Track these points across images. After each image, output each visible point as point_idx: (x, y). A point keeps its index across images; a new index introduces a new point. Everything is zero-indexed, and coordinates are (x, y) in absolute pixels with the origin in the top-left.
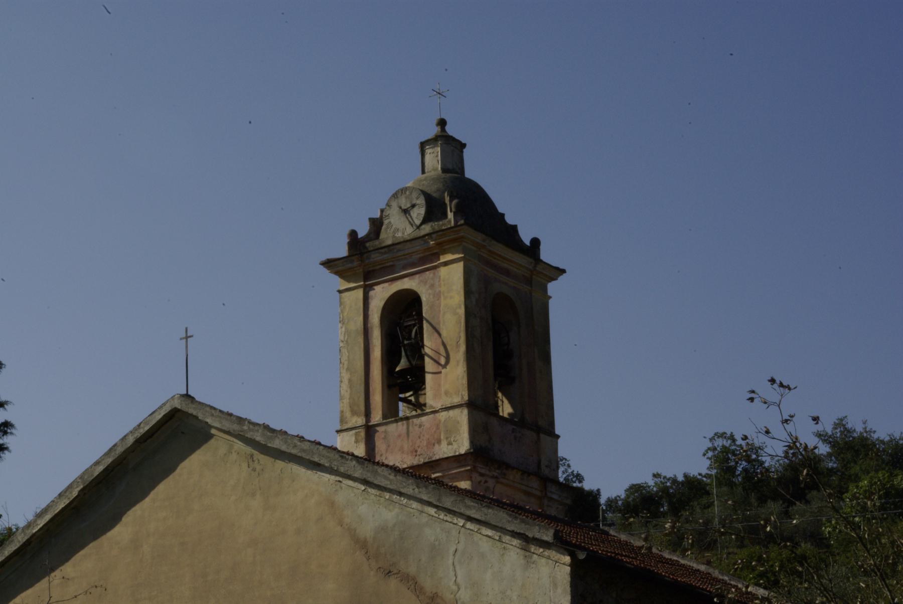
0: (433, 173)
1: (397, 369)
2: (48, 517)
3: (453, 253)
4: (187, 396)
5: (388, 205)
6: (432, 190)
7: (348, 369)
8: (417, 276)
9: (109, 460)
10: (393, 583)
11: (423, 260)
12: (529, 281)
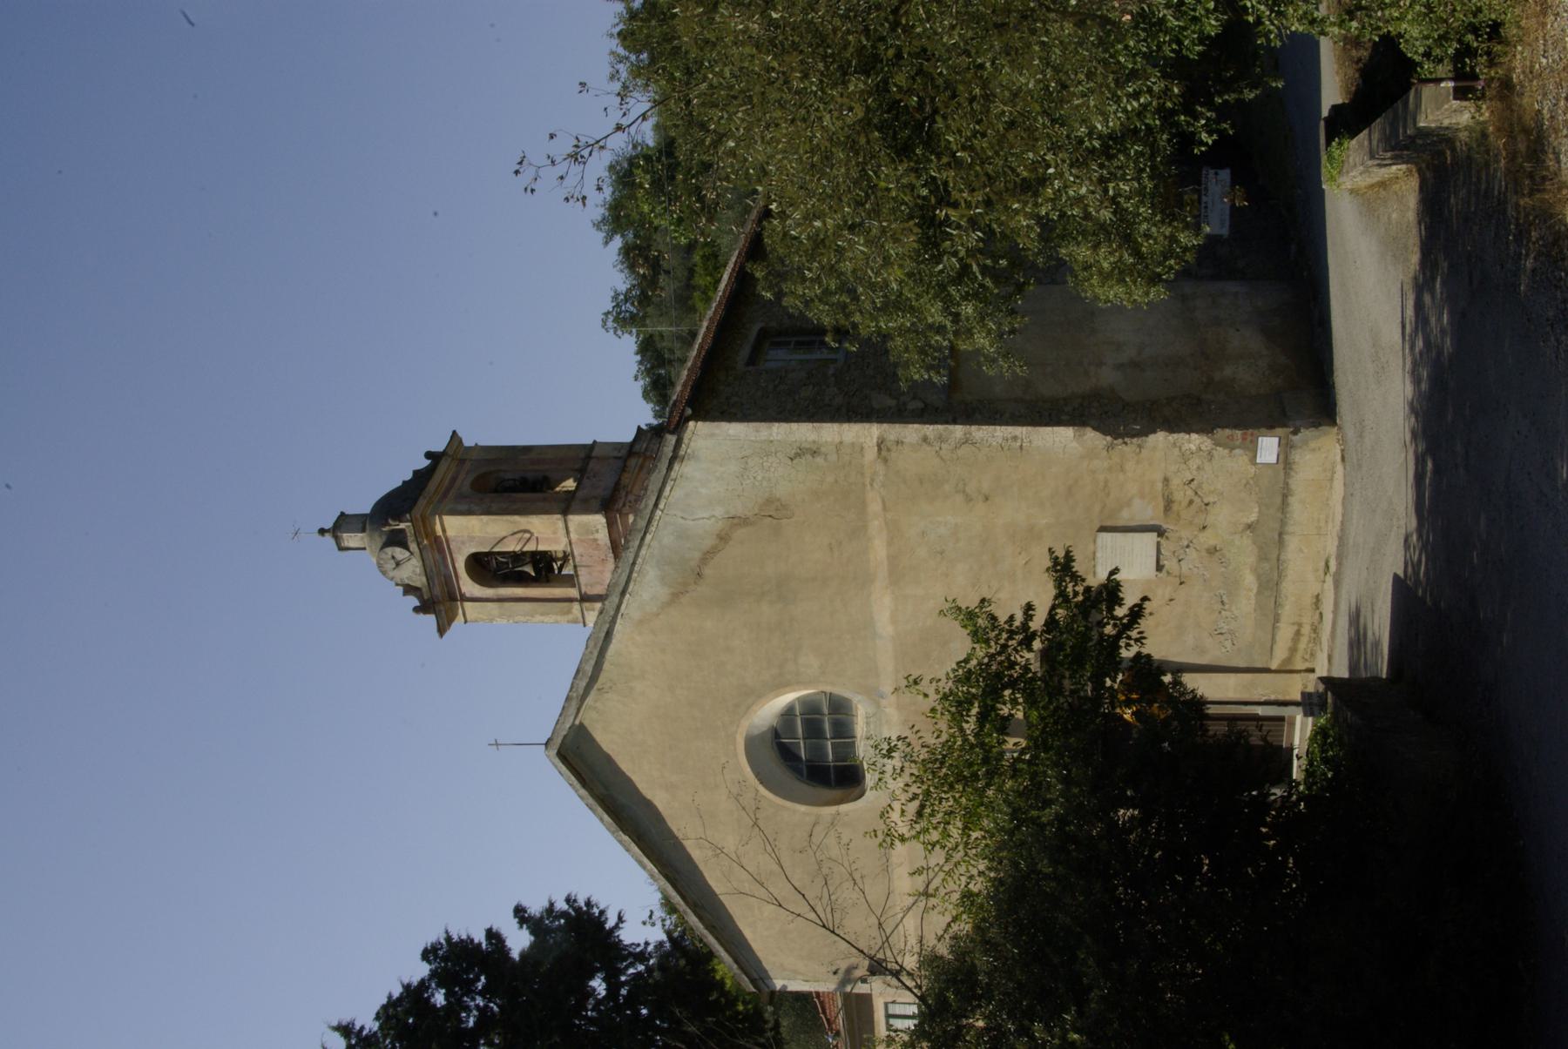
0: (366, 540)
1: (533, 574)
2: (646, 861)
3: (435, 524)
4: (546, 744)
5: (392, 579)
6: (379, 541)
7: (533, 616)
8: (454, 555)
9: (600, 810)
10: (707, 571)
11: (441, 551)
12: (462, 461)
